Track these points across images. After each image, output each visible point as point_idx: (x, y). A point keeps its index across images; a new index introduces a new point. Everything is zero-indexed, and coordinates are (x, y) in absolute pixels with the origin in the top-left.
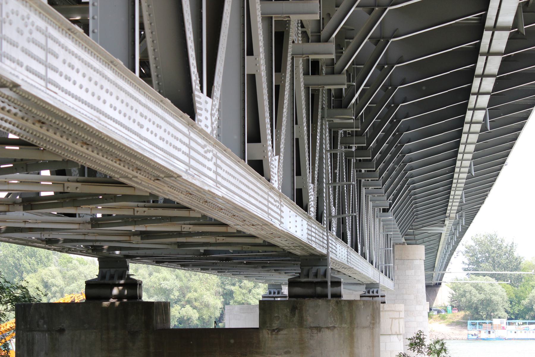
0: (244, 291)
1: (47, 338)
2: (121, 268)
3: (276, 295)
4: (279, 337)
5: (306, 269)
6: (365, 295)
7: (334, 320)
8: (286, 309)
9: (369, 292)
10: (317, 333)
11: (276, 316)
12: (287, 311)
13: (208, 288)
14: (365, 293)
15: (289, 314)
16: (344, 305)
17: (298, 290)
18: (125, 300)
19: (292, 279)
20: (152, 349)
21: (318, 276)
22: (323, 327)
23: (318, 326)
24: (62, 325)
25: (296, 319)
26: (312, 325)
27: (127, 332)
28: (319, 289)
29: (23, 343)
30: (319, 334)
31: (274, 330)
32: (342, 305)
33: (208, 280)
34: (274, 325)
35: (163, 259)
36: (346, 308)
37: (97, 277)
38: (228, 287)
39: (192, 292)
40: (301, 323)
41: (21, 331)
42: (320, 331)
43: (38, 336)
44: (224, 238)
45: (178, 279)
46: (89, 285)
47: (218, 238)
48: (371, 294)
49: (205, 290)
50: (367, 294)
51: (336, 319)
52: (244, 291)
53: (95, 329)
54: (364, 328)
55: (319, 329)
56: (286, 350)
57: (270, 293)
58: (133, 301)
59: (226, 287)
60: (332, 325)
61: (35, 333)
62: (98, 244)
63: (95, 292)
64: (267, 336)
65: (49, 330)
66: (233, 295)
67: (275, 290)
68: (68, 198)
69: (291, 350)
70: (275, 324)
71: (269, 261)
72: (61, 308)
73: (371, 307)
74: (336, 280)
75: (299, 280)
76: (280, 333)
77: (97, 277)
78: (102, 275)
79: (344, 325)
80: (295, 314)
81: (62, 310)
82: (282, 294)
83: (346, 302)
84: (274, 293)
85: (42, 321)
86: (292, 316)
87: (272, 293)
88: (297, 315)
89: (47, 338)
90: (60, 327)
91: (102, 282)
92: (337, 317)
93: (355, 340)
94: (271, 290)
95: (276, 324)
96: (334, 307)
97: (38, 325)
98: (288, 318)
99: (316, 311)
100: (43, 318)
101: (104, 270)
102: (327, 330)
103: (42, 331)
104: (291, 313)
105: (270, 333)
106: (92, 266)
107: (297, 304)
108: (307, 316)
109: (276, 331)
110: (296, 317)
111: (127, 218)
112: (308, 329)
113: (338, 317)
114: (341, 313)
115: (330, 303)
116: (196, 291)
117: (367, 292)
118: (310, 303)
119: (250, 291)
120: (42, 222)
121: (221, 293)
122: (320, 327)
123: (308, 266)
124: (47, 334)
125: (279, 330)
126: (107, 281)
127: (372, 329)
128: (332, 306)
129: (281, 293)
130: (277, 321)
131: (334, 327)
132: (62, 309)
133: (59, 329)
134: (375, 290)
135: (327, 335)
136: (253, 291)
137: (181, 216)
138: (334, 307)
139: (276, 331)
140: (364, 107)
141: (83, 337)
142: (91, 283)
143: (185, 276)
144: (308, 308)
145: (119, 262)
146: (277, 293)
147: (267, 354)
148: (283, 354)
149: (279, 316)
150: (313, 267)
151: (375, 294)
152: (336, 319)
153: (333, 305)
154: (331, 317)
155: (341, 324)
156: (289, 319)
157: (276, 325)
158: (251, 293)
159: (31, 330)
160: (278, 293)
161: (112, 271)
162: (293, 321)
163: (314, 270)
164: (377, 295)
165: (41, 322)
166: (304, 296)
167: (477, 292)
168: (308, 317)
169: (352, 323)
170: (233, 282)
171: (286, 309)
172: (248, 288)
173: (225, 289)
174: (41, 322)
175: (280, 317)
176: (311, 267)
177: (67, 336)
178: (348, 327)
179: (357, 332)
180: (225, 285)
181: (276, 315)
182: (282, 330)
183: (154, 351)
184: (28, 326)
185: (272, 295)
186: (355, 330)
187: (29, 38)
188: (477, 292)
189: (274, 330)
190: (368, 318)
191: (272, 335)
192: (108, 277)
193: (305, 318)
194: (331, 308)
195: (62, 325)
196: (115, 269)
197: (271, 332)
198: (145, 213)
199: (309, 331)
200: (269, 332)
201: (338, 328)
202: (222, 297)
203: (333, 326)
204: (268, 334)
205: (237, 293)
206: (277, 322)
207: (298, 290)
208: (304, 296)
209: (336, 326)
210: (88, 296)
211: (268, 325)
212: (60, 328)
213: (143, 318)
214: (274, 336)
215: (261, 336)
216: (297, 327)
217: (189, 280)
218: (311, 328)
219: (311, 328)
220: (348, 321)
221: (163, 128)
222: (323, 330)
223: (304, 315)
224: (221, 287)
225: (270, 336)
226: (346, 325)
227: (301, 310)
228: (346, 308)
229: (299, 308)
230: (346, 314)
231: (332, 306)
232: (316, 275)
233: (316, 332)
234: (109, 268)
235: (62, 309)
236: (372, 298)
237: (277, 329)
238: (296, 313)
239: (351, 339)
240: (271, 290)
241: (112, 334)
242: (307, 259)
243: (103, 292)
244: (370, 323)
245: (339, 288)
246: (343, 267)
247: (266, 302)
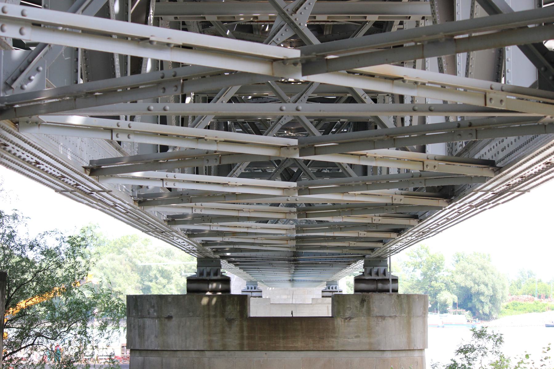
0: (160, 286)
1: (157, 324)
2: (214, 267)
3: (253, 290)
4: (351, 324)
5: (369, 269)
6: (326, 290)
7: (396, 310)
8: (357, 301)
9: (329, 288)
10: (382, 321)
12: (357, 303)
13: (130, 283)
14: (326, 289)
15: (359, 305)
17: (363, 286)
18: (220, 293)
19: (358, 277)
20: (245, 334)
21: (379, 274)
22: (387, 316)
23: (382, 315)
24: (170, 313)
25: (364, 309)
26: (378, 315)
27: (225, 319)
28: (380, 286)
29: (134, 327)
30: (384, 322)
31: (346, 319)
33: (131, 277)
34: (346, 314)
35: (252, 260)
36: (405, 301)
37: (195, 274)
38: (147, 283)
39: (117, 287)
40: (369, 312)
41: (133, 318)
42: (384, 319)
43: (148, 322)
44: (355, 243)
45: (105, 276)
46: (190, 280)
47: (351, 242)
48: (331, 290)
49: (127, 285)
50: (328, 290)
51: (397, 309)
52: (160, 286)
53: (198, 317)
54: (418, 317)
55: (383, 317)
56: (356, 335)
57: (248, 288)
58: (227, 294)
59: (145, 283)
60: (394, 315)
61: (146, 319)
62: (385, 245)
63: (195, 286)
64: (340, 323)
65: (158, 317)
66: (150, 290)
67: (252, 286)
68: (347, 208)
69: (360, 335)
70: (348, 313)
71: (320, 262)
72: (169, 299)
74: (394, 278)
75: (363, 277)
76: (351, 320)
77: (195, 274)
78: (201, 273)
79: (403, 315)
81: (170, 301)
82: (258, 289)
83: (405, 296)
84: (251, 288)
85: (153, 310)
87: (250, 288)
89: (157, 324)
90: (168, 314)
91: (201, 278)
92: (398, 308)
93: (412, 327)
94: (248, 286)
95: (348, 314)
97: (149, 313)
99: (381, 303)
100: (153, 307)
101: (202, 268)
102: (390, 318)
103: (153, 318)
104: (361, 304)
105: (343, 321)
108: (373, 308)
109: (348, 319)
111: (333, 226)
112: (375, 318)
113: (399, 308)
114: (401, 305)
116: (120, 286)
117: (327, 288)
118: (376, 296)
119: (164, 287)
120: (261, 228)
121: (141, 288)
122: (384, 316)
123: (370, 266)
124: (157, 321)
125: (350, 318)
126: (205, 277)
127: (424, 318)
128: (394, 299)
129: (257, 289)
130: (349, 311)
131: (396, 316)
132: (170, 299)
133: (167, 316)
134: (334, 287)
135: (390, 323)
136: (167, 286)
139: (348, 319)
141: (188, 323)
142: (191, 279)
143: (111, 274)
144: (374, 301)
145: (214, 261)
146: (253, 288)
147: (341, 338)
148: (354, 338)
149: (350, 307)
150: (374, 267)
151: (334, 290)
152: (397, 309)
153: (395, 298)
155: (401, 314)
156: (359, 309)
157: (348, 314)
158: (165, 288)
159: (142, 317)
160: (255, 288)
161: (208, 269)
162: (362, 311)
163: (375, 269)
164: (336, 290)
165: (152, 310)
166: (368, 291)
167: (350, 288)
168: (375, 308)
169: (409, 313)
170: (151, 279)
172: (163, 284)
173: (143, 285)
174: (152, 310)
175: (352, 307)
176: (373, 267)
177: (174, 322)
178: (406, 317)
179: (413, 320)
180: (144, 281)
181: (348, 306)
182: (353, 318)
183: (247, 335)
184: (140, 314)
185: (250, 290)
186: (412, 319)
188: (350, 288)
189: (346, 319)
190: (421, 309)
191: (345, 322)
192: (205, 274)
193: (372, 308)
194: (393, 301)
195: (170, 313)
196: (210, 268)
197: (344, 320)
198: (380, 221)
199: (376, 319)
200: (343, 320)
201: (399, 317)
202: (141, 291)
203: (395, 316)
204: (342, 322)
205: (154, 288)
206: (349, 312)
207: (363, 286)
208: (368, 291)
209: (397, 315)
210: (189, 291)
211: (342, 314)
212: (169, 316)
213: (238, 307)
214: (346, 323)
215: (336, 323)
216: (366, 316)
217: (114, 277)
218: (377, 317)
219: (377, 317)
220: (407, 311)
221: (500, 152)
222: (386, 318)
223: (371, 306)
224: (141, 283)
225: (343, 323)
226: (405, 315)
227: (369, 302)
228: (405, 301)
229: (367, 301)
230: (405, 306)
231: (394, 299)
232: (377, 274)
233: (381, 320)
234: (205, 266)
235: (170, 299)
236: (331, 293)
237: (349, 317)
239: (409, 325)
240: (248, 286)
241: (212, 320)
242: (370, 261)
243: (202, 286)
244: (423, 313)
245: (396, 284)
246: (230, 267)
247: (340, 295)
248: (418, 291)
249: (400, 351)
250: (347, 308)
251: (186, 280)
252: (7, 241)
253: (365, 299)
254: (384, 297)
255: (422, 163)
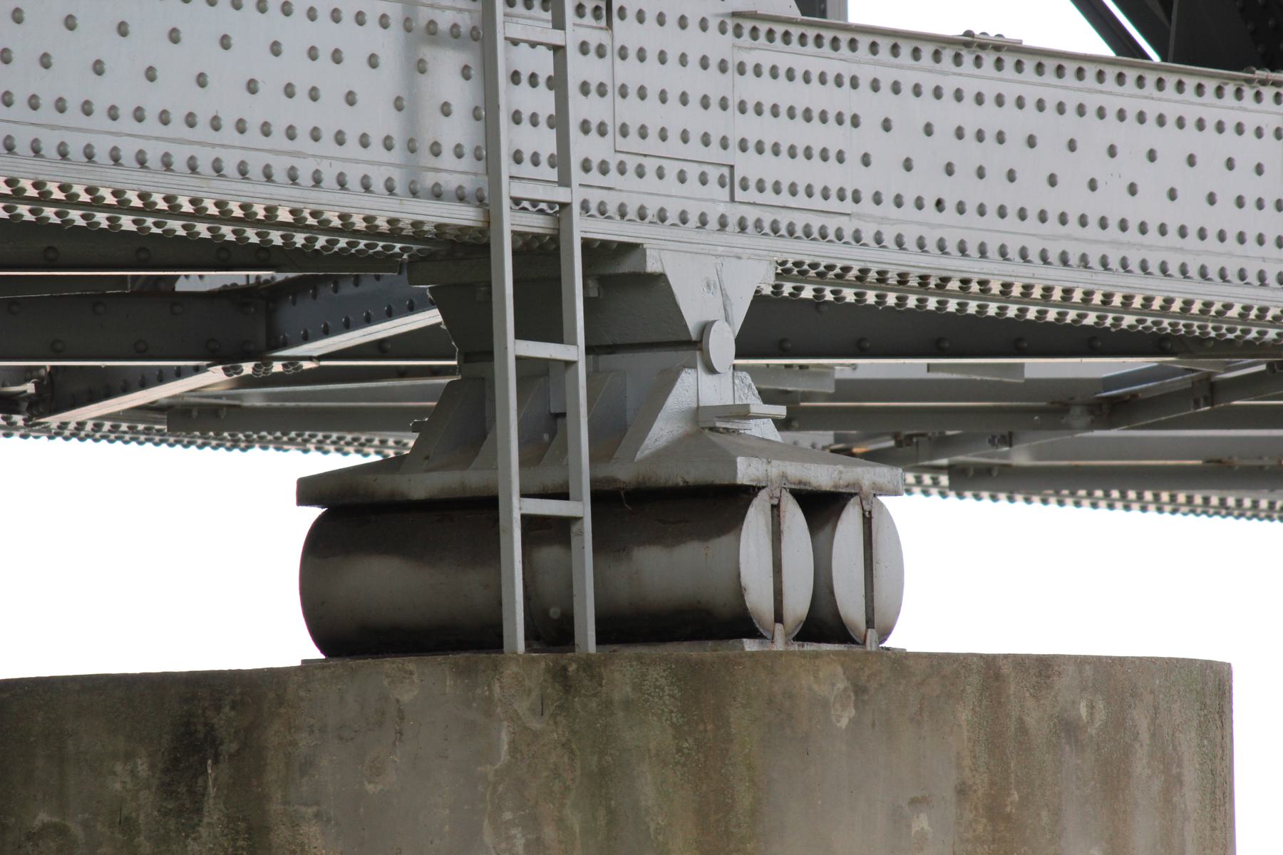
8: (129, 756)
11: (45, 827)
16: (627, 704)
32: (608, 704)
51: (549, 833)
56: (378, 449)
73: (964, 715)
80: (197, 797)
86: (172, 824)
88: (213, 812)
92: (560, 822)
96: (536, 725)
98: (1217, 722)
104: (167, 790)
106: (653, 675)
107: (218, 709)
108: (295, 825)
110: (203, 831)
115: (497, 688)
137: (543, 500)
138: (536, 725)
140: (1125, 387)
144: (304, 741)
149: (61, 831)
152: (549, 833)
154: (508, 816)
171: (129, 756)
175: (76, 830)
181: (43, 817)
187: (301, 211)
194: (505, 738)
223: (275, 807)
238: (212, 791)
248: (1141, 745)
249: (804, 211)
250: (30, 836)
251: (576, 641)
252: (882, 664)
253: (211, 729)
254: (407, 695)
255: (617, 149)
